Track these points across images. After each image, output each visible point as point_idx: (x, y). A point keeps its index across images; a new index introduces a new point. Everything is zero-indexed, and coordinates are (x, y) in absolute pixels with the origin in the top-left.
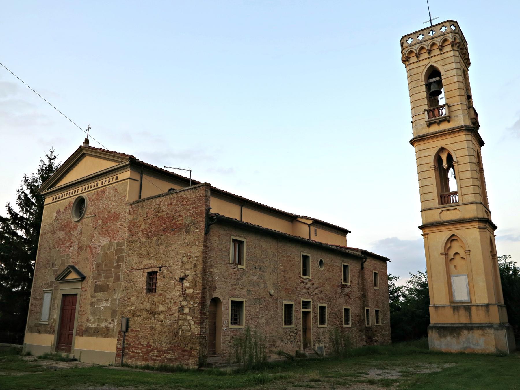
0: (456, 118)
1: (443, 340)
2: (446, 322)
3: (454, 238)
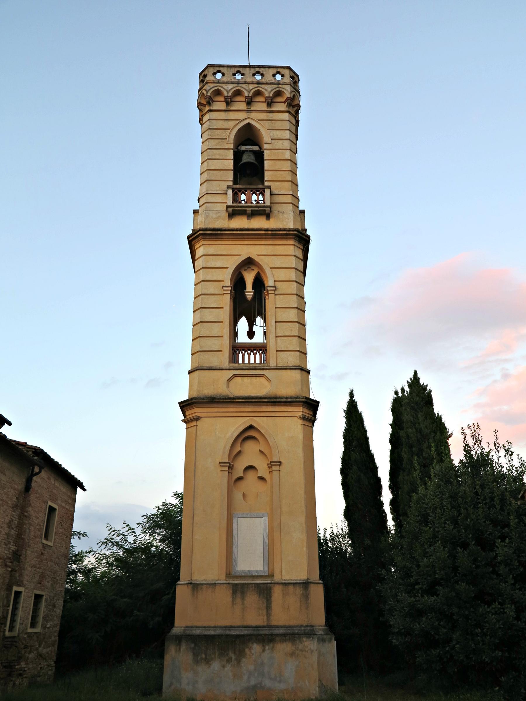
0: (281, 214)
1: (202, 669)
2: (212, 624)
3: (251, 433)
